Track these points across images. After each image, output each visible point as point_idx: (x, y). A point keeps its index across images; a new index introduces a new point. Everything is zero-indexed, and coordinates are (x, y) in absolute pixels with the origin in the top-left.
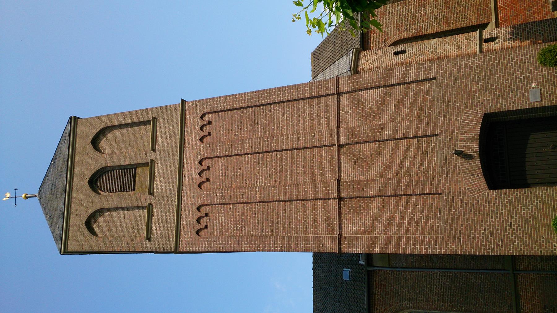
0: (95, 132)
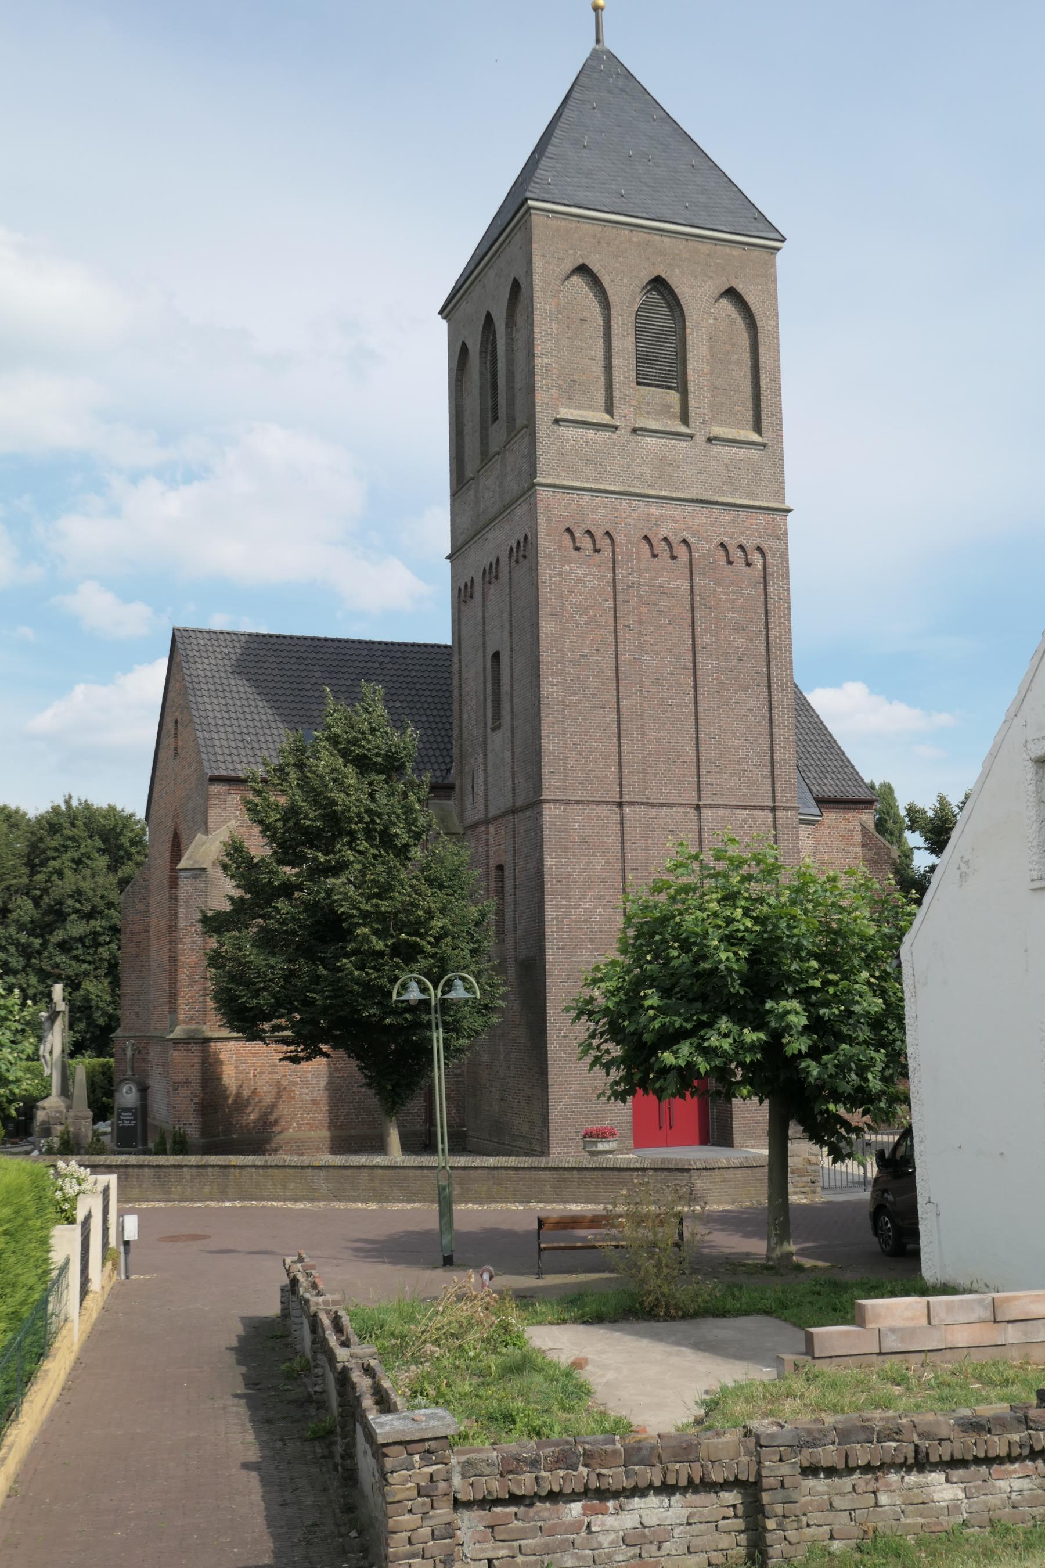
0: (750, 299)
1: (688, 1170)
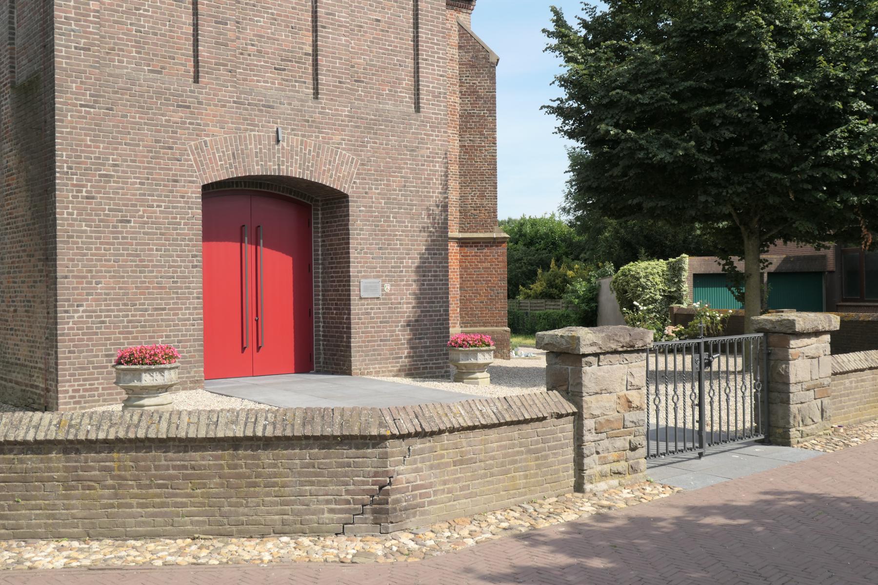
1: (383, 438)
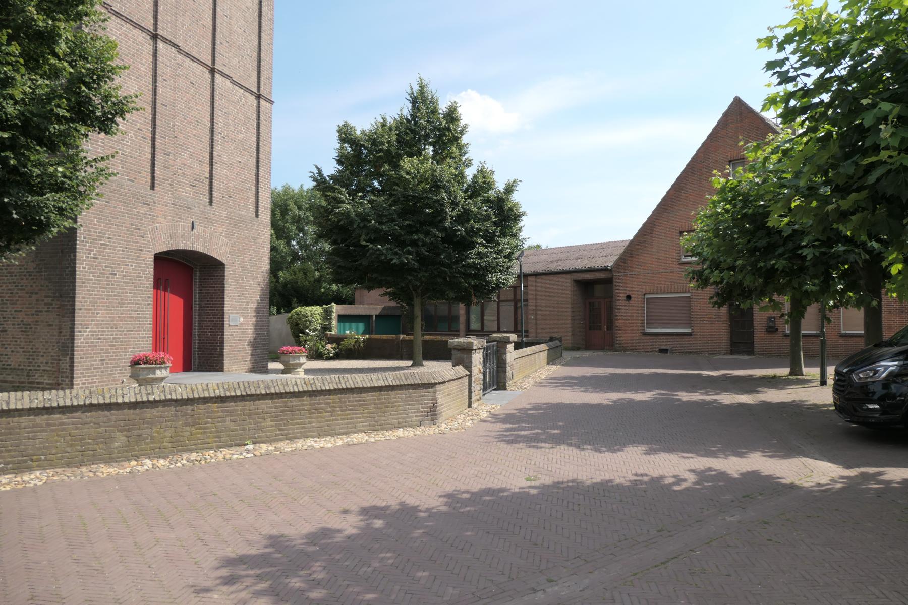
1: (436, 384)
